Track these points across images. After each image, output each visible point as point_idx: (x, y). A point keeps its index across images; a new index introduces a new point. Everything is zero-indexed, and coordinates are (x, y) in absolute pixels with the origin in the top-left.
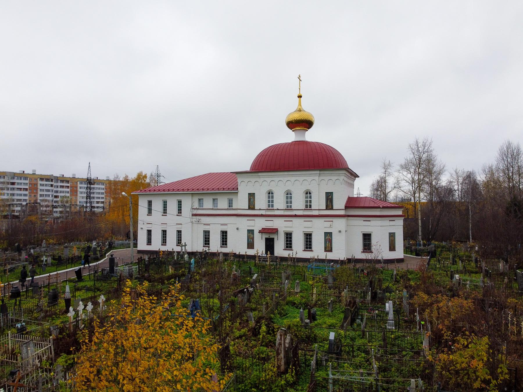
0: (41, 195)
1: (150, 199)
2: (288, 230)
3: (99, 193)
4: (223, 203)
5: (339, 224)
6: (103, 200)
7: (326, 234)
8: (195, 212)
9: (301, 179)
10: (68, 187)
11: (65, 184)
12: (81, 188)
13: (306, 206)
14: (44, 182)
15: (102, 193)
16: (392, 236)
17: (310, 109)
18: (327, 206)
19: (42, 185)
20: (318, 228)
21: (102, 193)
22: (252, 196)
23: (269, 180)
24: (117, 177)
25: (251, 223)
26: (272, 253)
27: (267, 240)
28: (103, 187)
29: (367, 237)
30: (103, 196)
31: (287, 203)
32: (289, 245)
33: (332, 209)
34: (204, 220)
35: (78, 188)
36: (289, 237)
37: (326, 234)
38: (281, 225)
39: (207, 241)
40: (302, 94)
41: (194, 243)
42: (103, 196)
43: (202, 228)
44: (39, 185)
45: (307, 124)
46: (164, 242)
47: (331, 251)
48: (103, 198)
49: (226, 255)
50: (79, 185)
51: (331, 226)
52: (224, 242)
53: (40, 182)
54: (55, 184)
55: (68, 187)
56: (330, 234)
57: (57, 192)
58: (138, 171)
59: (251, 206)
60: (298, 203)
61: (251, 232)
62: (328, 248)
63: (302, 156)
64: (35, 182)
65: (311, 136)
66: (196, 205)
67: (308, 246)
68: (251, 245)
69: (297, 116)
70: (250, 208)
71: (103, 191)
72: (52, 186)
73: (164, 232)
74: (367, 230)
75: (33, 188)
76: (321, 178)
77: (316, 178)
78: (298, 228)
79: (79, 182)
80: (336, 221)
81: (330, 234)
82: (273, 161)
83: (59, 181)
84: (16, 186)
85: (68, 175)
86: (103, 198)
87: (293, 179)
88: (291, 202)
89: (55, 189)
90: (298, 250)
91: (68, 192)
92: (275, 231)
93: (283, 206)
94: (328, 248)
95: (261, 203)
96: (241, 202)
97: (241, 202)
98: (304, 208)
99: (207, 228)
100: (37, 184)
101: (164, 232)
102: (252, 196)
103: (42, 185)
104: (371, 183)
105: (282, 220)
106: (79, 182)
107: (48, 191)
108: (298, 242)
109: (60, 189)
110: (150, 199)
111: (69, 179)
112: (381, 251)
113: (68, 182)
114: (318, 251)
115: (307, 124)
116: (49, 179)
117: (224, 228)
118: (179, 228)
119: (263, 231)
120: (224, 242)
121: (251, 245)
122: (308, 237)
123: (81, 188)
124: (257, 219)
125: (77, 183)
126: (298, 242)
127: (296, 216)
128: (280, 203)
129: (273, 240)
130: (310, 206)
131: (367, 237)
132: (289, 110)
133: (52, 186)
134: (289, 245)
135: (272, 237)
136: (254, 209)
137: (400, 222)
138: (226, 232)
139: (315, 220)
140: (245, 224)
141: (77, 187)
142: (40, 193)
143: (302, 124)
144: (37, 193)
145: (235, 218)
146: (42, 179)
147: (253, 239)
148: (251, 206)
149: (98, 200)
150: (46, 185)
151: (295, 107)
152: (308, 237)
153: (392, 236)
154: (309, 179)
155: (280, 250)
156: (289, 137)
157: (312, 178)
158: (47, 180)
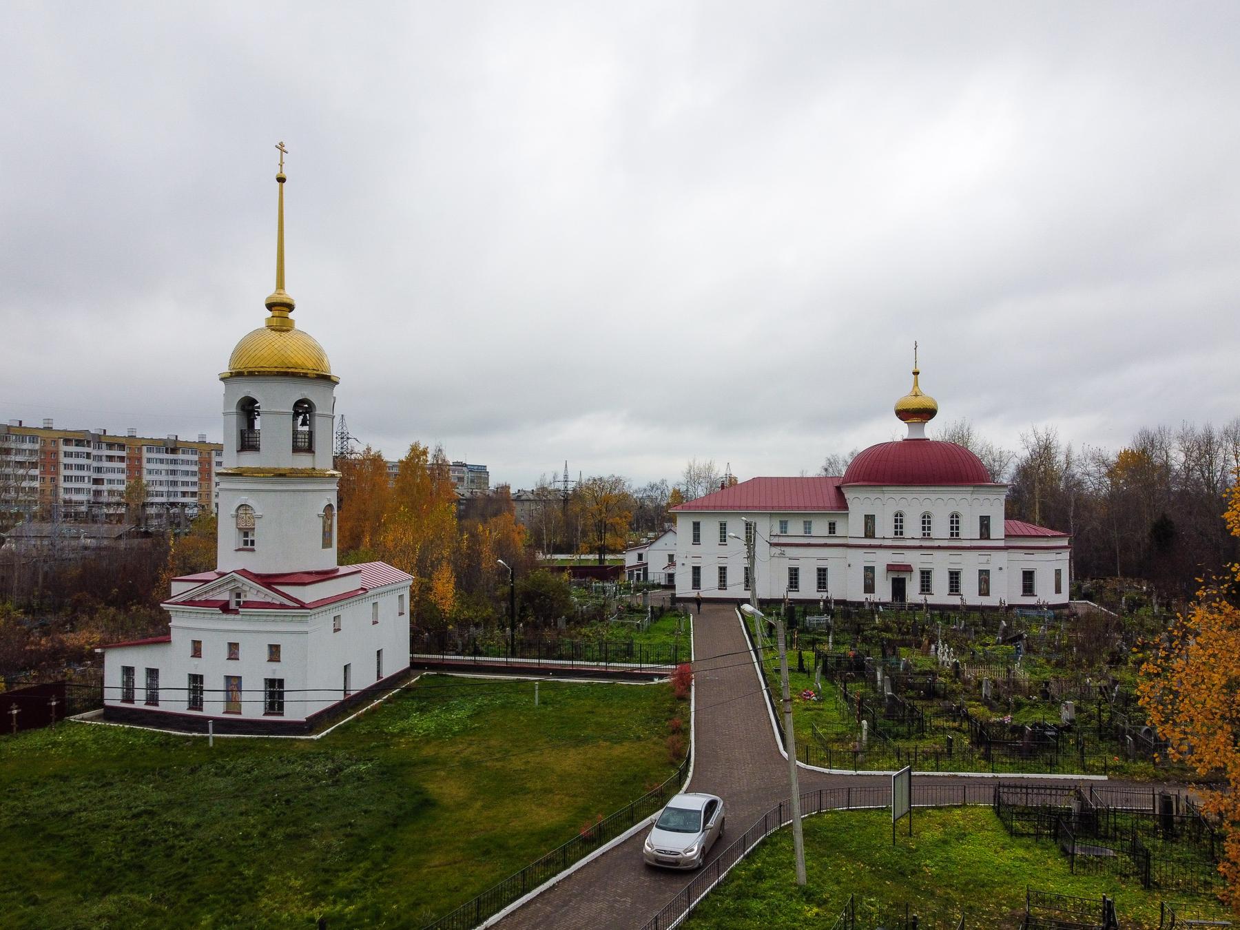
0: (67, 479)
1: (696, 520)
2: (926, 567)
3: (187, 473)
4: (820, 528)
5: (999, 558)
6: (195, 489)
7: (981, 572)
8: (775, 540)
9: (945, 497)
10: (122, 459)
11: (116, 453)
12: (149, 460)
13: (952, 534)
14: (72, 449)
15: (194, 473)
16: (1058, 573)
17: (930, 393)
18: (981, 535)
19: (67, 454)
20: (969, 565)
21: (194, 473)
22: (870, 520)
23: (897, 497)
26: (903, 598)
27: (894, 580)
28: (196, 458)
29: (1028, 576)
30: (195, 479)
31: (924, 529)
32: (926, 587)
33: (988, 538)
34: (790, 552)
35: (144, 461)
36: (926, 576)
37: (981, 572)
38: (916, 560)
40: (285, 174)
44: (62, 455)
48: (194, 484)
49: (827, 602)
50: (146, 454)
52: (822, 583)
53: (64, 448)
54: (95, 452)
55: (122, 459)
56: (987, 572)
57: (99, 470)
59: (870, 533)
60: (941, 530)
61: (869, 571)
62: (984, 591)
64: (51, 447)
65: (933, 431)
66: (777, 530)
68: (869, 588)
69: (915, 403)
70: (866, 536)
71: (196, 468)
72: (88, 456)
74: (1029, 566)
75: (49, 462)
76: (975, 496)
77: (968, 496)
79: (145, 448)
81: (987, 572)
82: (882, 469)
83: (104, 446)
84: (13, 458)
86: (194, 484)
88: (929, 529)
89: (95, 464)
90: (940, 595)
92: (908, 569)
93: (890, 532)
94: (984, 591)
95: (884, 528)
96: (853, 527)
98: (948, 536)
99: (794, 564)
100: (56, 453)
102: (870, 520)
103: (67, 454)
104: (701, 462)
105: (917, 553)
106: (145, 448)
107: (81, 467)
108: (940, 583)
109: (106, 464)
112: (1046, 594)
113: (122, 447)
114: (970, 595)
116: (79, 439)
117: (822, 564)
118: (723, 563)
119: (891, 568)
120: (822, 583)
121: (869, 588)
122: (954, 577)
123: (149, 460)
124: (880, 552)
125: (140, 449)
126: (940, 583)
128: (913, 529)
130: (957, 534)
131: (1028, 576)
132: (902, 394)
133: (88, 456)
134: (926, 587)
137: (1066, 555)
140: (860, 559)
142: (64, 472)
143: (919, 414)
144: (57, 473)
145: (841, 549)
146: (67, 442)
148: (870, 533)
149: (185, 489)
150: (78, 455)
151: (908, 389)
152: (954, 577)
153: (1058, 573)
155: (913, 594)
156: (900, 431)
157: (961, 496)
158: (79, 443)
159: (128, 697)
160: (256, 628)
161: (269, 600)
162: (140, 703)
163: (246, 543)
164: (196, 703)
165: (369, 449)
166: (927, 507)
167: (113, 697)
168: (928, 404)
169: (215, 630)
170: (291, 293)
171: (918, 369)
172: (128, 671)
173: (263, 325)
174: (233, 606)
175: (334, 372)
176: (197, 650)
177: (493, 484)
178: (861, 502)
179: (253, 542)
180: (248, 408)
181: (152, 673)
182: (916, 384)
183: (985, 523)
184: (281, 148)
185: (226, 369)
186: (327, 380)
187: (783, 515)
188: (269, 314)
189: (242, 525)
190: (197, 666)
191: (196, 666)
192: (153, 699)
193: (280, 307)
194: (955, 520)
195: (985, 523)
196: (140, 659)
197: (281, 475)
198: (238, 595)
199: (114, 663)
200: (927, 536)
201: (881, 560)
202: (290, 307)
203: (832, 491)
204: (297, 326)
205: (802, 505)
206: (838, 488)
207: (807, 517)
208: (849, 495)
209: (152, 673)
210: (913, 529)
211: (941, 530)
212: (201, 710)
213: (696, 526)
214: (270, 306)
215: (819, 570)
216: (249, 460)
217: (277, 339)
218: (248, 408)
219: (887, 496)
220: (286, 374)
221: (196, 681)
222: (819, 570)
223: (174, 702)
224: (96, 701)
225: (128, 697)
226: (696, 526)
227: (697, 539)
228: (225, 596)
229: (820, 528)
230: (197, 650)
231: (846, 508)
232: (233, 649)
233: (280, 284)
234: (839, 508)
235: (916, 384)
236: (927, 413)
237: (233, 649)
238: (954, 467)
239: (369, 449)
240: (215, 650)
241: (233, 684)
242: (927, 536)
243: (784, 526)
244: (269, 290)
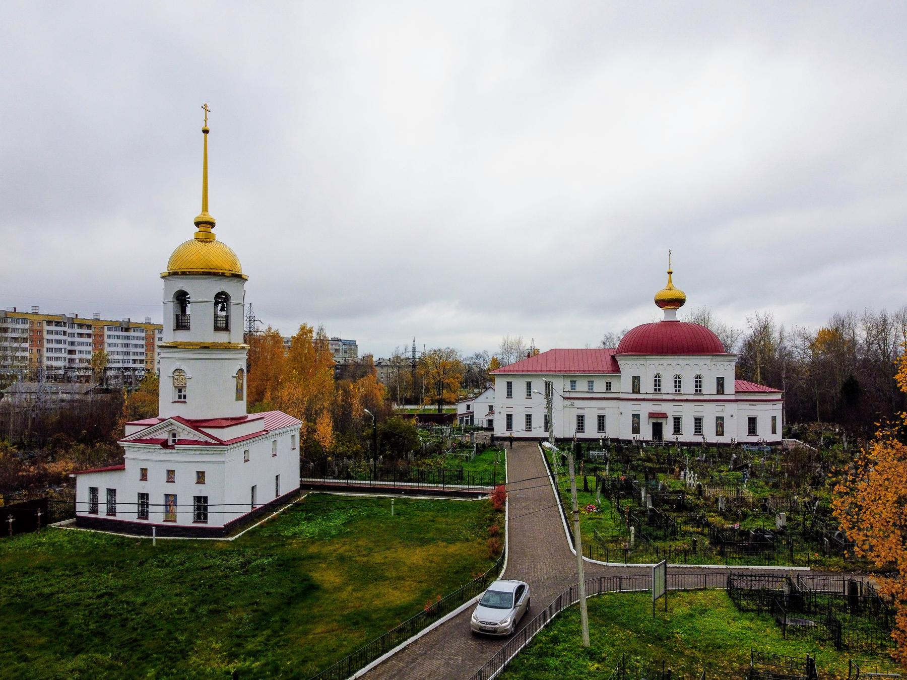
0: (49, 350)
2: (677, 414)
3: (136, 346)
4: (600, 386)
6: (143, 358)
8: (567, 395)
10: (89, 335)
11: (85, 331)
12: (109, 337)
13: (696, 391)
14: (53, 328)
15: (142, 346)
17: (680, 288)
18: (718, 391)
21: (142, 346)
22: (636, 380)
23: (656, 363)
25: (636, 407)
26: (660, 437)
28: (143, 335)
29: (752, 421)
31: (676, 386)
32: (677, 429)
33: (723, 393)
34: (578, 403)
35: (105, 337)
36: (677, 421)
37: (717, 418)
38: (670, 410)
39: (581, 426)
40: (209, 127)
42: (143, 350)
43: (575, 413)
44: (45, 333)
47: (722, 434)
48: (142, 354)
50: (106, 332)
51: (722, 411)
53: (46, 328)
54: (69, 331)
55: (89, 335)
56: (722, 418)
57: (72, 343)
59: (636, 389)
60: (688, 387)
61: (636, 417)
62: (720, 432)
64: (37, 327)
65: (682, 315)
66: (568, 388)
67: (698, 429)
68: (636, 430)
70: (634, 392)
71: (143, 342)
72: (65, 333)
73: (529, 417)
74: (752, 414)
76: (713, 363)
77: (708, 363)
78: (688, 413)
79: (106, 328)
80: (728, 406)
81: (722, 418)
83: (76, 326)
85: (86, 315)
86: (142, 354)
88: (680, 387)
90: (688, 435)
91: (90, 345)
92: (664, 416)
93: (651, 389)
94: (720, 432)
95: (647, 386)
96: (623, 385)
97: (623, 385)
99: (581, 412)
100: (41, 331)
101: (529, 417)
102: (636, 380)
104: (513, 338)
105: (671, 404)
106: (106, 328)
107: (59, 342)
108: (688, 426)
110: (529, 380)
111: (90, 323)
112: (765, 434)
113: (89, 327)
115: (678, 302)
117: (601, 413)
118: (529, 412)
119: (652, 415)
120: (601, 426)
121: (636, 430)
122: (698, 422)
123: (109, 337)
124: (643, 404)
125: (102, 328)
126: (688, 426)
127: (644, 400)
128: (667, 386)
129: (661, 424)
130: (700, 391)
131: (752, 421)
132: (660, 289)
134: (677, 429)
135: (659, 421)
136: (638, 392)
137: (780, 406)
139: (706, 405)
140: (629, 409)
141: (102, 336)
142: (46, 345)
146: (49, 323)
147: (638, 424)
148: (636, 389)
149: (135, 357)
150: (57, 333)
152: (698, 422)
154: (701, 363)
155: (668, 434)
156: (658, 315)
157: (703, 363)
158: (58, 324)
159: (94, 510)
160: (187, 459)
161: (197, 438)
162: (102, 515)
163: (180, 397)
164: (143, 514)
166: (678, 371)
167: (83, 509)
168: (678, 296)
169: (157, 461)
170: (212, 215)
171: (672, 270)
172: (94, 491)
173: (193, 237)
174: (170, 443)
175: (244, 272)
176: (144, 475)
178: (630, 367)
179: (185, 397)
180: (182, 298)
181: (112, 492)
182: (670, 281)
183: (720, 382)
184: (205, 108)
185: (165, 270)
187: (573, 376)
188: (197, 230)
189: (177, 384)
190: (144, 487)
191: (144, 487)
192: (112, 511)
194: (698, 380)
195: (720, 382)
196: (103, 481)
197: (205, 348)
199: (84, 484)
200: (678, 392)
201: (644, 410)
202: (212, 225)
204: (217, 238)
206: (613, 357)
207: (590, 376)
208: (621, 362)
209: (112, 492)
211: (688, 387)
212: (147, 519)
213: (509, 385)
214: (198, 224)
215: (599, 417)
216: (182, 337)
217: (203, 248)
218: (182, 298)
219: (649, 363)
220: (209, 274)
222: (599, 417)
223: (127, 513)
224: (70, 512)
225: (94, 510)
226: (509, 385)
227: (509, 394)
228: (164, 436)
229: (600, 386)
230: (144, 475)
231: (619, 371)
232: (201, 477)
233: (205, 207)
239: (270, 328)
240: (157, 475)
241: (171, 500)
242: (678, 392)
243: (573, 384)
244: (196, 212)
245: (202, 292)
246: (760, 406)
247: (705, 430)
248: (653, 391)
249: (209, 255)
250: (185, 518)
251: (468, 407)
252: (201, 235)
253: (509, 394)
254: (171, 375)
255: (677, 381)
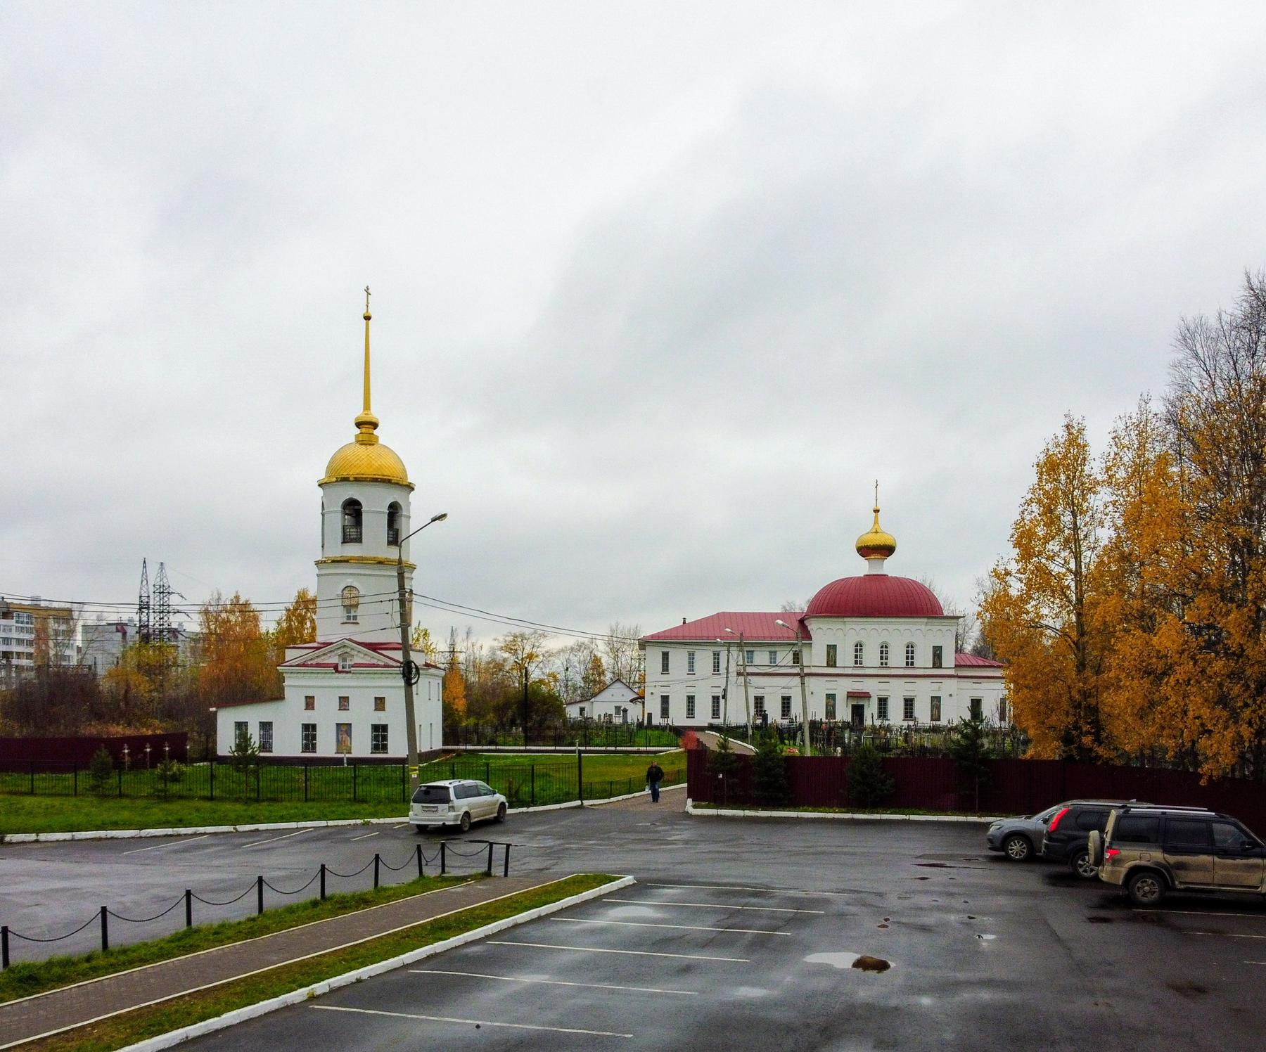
1: (665, 650)
2: (883, 694)
9: (902, 628)
20: (923, 692)
22: (832, 649)
23: (858, 627)
24: (219, 599)
25: (830, 685)
32: (883, 713)
33: (940, 667)
36: (883, 702)
38: (874, 687)
40: (371, 313)
41: (738, 713)
45: (887, 550)
46: (691, 712)
58: (300, 587)
59: (831, 662)
60: (897, 658)
63: (879, 597)
65: (891, 567)
70: (828, 666)
73: (691, 700)
74: (976, 695)
78: (896, 692)
80: (947, 682)
82: (842, 602)
87: (891, 627)
92: (867, 696)
95: (845, 658)
96: (815, 657)
101: (691, 700)
102: (832, 649)
118: (691, 692)
119: (850, 695)
128: (871, 658)
129: (862, 706)
132: (862, 530)
138: (314, 727)
139: (918, 681)
147: (834, 706)
148: (831, 662)
149: (21, 636)
151: (869, 526)
155: (871, 716)
156: (861, 567)
160: (364, 684)
161: (374, 661)
163: (349, 617)
165: (237, 598)
166: (885, 638)
168: (888, 543)
169: (327, 688)
170: (375, 414)
171: (879, 507)
173: (353, 440)
174: (340, 668)
175: (411, 479)
176: (310, 703)
177: (1213, 322)
178: (824, 632)
179: (355, 617)
180: (353, 509)
182: (876, 522)
183: (937, 653)
184: (367, 290)
185: (322, 475)
186: (410, 488)
187: (746, 644)
188: (358, 431)
189: (347, 602)
190: (309, 717)
193: (367, 425)
194: (910, 649)
195: (937, 653)
196: (253, 715)
197: (380, 563)
198: (344, 660)
199: (226, 721)
200: (884, 665)
202: (375, 425)
203: (796, 625)
204: (381, 441)
205: (767, 634)
207: (771, 645)
208: (813, 626)
209: (266, 727)
210: (871, 658)
211: (897, 658)
213: (665, 656)
214: (359, 425)
215: (783, 698)
216: (352, 550)
218: (353, 509)
219: (848, 627)
220: (375, 480)
221: (309, 731)
222: (783, 698)
224: (209, 753)
226: (665, 656)
227: (665, 668)
228: (334, 660)
229: (785, 657)
230: (310, 703)
231: (810, 638)
232: (344, 702)
233: (367, 406)
234: (803, 639)
235: (876, 522)
236: (887, 550)
237: (344, 702)
238: (913, 603)
239: (237, 598)
241: (344, 730)
242: (884, 665)
244: (358, 412)
245: (375, 503)
246: (986, 685)
247: (917, 713)
248: (853, 664)
249: (365, 460)
250: (361, 747)
251: (582, 710)
252: (365, 437)
253: (665, 668)
254: (340, 592)
255: (884, 650)
